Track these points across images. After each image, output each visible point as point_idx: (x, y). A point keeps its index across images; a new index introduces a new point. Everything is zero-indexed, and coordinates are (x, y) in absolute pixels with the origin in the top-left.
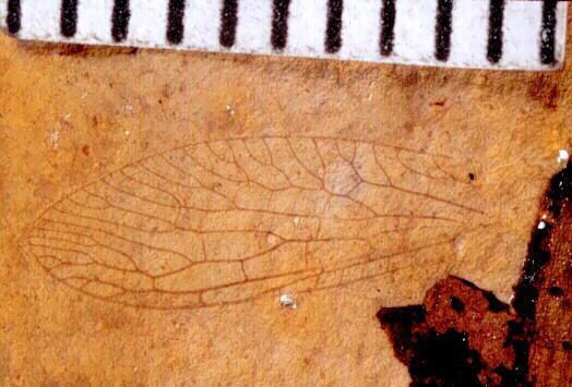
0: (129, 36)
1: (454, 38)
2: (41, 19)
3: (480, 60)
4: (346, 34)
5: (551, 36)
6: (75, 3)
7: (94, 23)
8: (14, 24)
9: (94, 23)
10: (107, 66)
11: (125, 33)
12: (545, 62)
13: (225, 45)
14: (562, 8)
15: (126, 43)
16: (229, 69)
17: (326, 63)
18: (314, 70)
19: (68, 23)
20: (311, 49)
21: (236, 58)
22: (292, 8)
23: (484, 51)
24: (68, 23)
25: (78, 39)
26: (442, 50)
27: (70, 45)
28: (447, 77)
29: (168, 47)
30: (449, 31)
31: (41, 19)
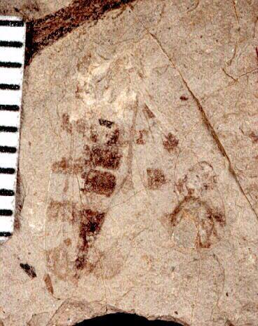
0: (12, 189)
1: (13, 61)
2: (5, 224)
3: (19, 93)
6: (2, 42)
7: (8, 182)
8: (8, 234)
9: (8, 182)
10: (22, 172)
16: (25, 129)
19: (7, 213)
22: (2, 61)
24: (7, 213)
25: (15, 190)
30: (9, 63)
31: (5, 224)
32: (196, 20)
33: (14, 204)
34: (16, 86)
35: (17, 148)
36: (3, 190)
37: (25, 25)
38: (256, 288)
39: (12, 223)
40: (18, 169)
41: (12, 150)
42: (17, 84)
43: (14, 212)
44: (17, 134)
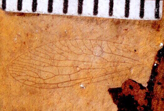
0: (37, 10)
1: (130, 11)
2: (12, 5)
3: (138, 17)
4: (99, 10)
5: (158, 10)
6: (22, 1)
7: (27, 7)
8: (4, 7)
9: (27, 7)
10: (31, 19)
11: (36, 9)
12: (156, 18)
13: (65, 13)
14: (161, 2)
15: (36, 12)
16: (66, 20)
17: (93, 18)
18: (90, 20)
19: (20, 7)
20: (89, 14)
21: (68, 17)
22: (84, 2)
23: (139, 15)
24: (20, 7)
25: (22, 11)
26: (127, 14)
27: (20, 13)
28: (128, 22)
29: (48, 14)
30: (129, 9)
31: (12, 5)
38: (66, 110)
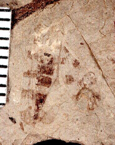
0: (5, 84)
1: (6, 27)
2: (2, 100)
3: (8, 41)
6: (1, 19)
7: (3, 81)
8: (4, 104)
9: (3, 81)
10: (10, 77)
16: (11, 58)
19: (3, 95)
22: (1, 27)
24: (3, 95)
25: (7, 85)
30: (4, 28)
31: (2, 100)
32: (87, 9)
33: (6, 91)
34: (7, 38)
35: (8, 66)
36: (1, 85)
37: (11, 11)
39: (5, 99)
40: (8, 75)
41: (5, 67)
42: (8, 37)
43: (6, 94)
44: (8, 60)
